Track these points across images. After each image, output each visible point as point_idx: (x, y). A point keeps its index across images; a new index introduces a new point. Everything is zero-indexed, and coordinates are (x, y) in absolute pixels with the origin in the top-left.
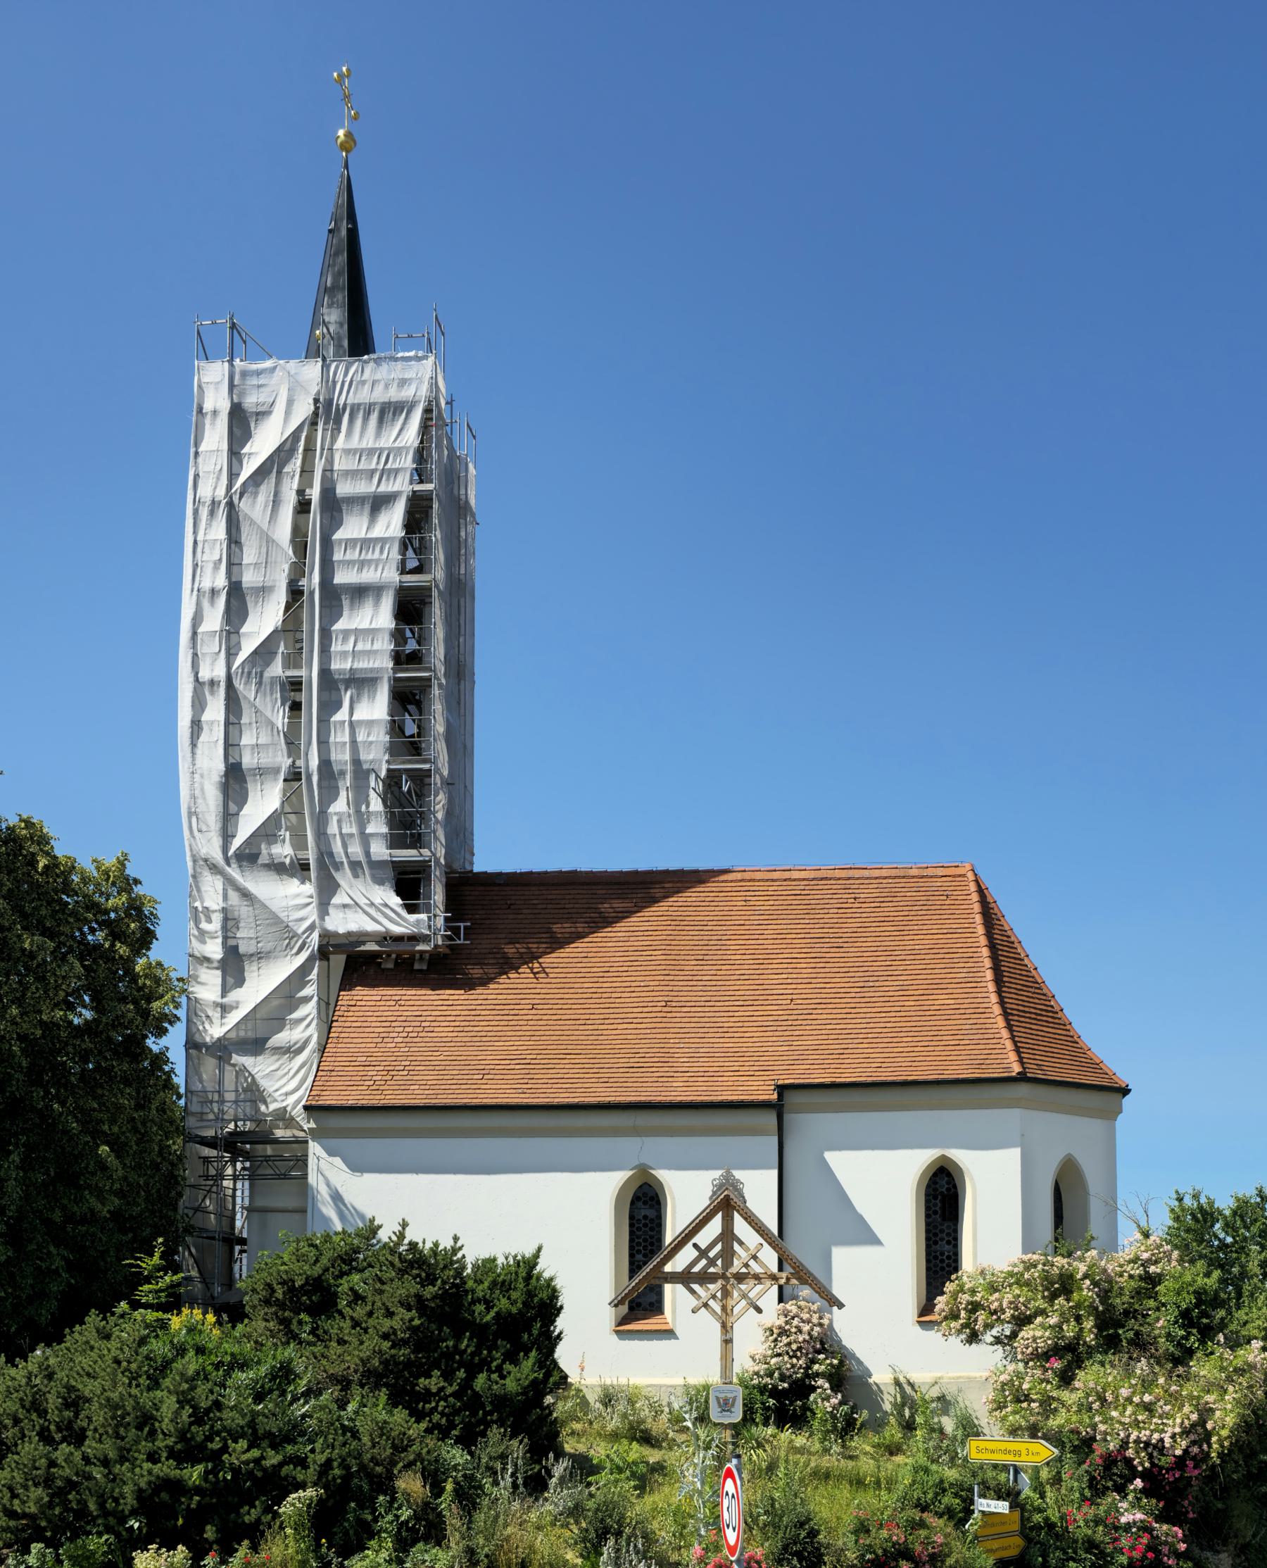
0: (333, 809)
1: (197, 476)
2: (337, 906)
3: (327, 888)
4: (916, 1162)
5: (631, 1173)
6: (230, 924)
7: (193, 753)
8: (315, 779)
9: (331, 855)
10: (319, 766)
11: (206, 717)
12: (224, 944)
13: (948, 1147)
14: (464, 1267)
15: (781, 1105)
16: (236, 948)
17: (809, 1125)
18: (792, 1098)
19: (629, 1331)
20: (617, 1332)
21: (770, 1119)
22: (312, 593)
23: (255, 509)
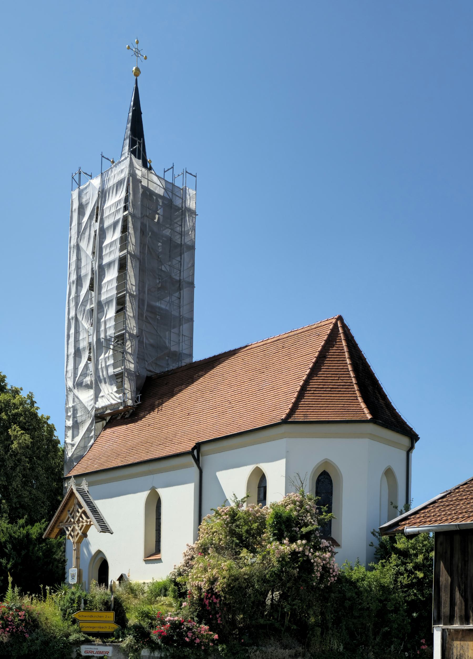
0: (100, 358)
1: (71, 237)
2: (100, 397)
3: (98, 392)
4: (247, 470)
5: (150, 491)
6: (75, 412)
7: (241, 348)
8: (95, 347)
9: (99, 377)
10: (96, 341)
11: (71, 333)
12: (73, 420)
13: (259, 463)
14: (352, 578)
15: (197, 452)
16: (77, 421)
17: (210, 459)
18: (204, 449)
19: (150, 560)
20: (145, 560)
21: (190, 459)
22: (96, 271)
23: (83, 245)
